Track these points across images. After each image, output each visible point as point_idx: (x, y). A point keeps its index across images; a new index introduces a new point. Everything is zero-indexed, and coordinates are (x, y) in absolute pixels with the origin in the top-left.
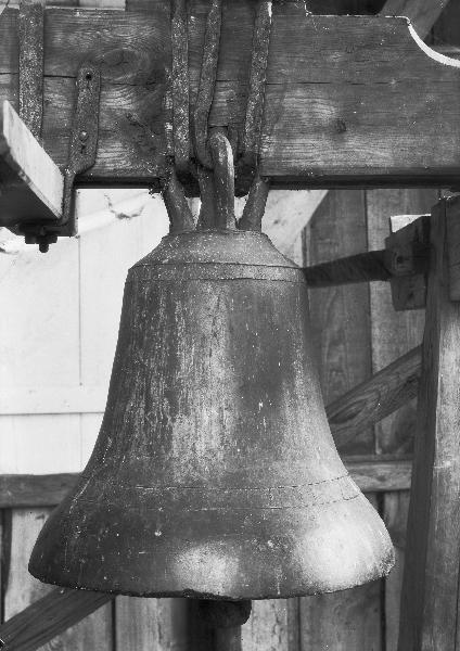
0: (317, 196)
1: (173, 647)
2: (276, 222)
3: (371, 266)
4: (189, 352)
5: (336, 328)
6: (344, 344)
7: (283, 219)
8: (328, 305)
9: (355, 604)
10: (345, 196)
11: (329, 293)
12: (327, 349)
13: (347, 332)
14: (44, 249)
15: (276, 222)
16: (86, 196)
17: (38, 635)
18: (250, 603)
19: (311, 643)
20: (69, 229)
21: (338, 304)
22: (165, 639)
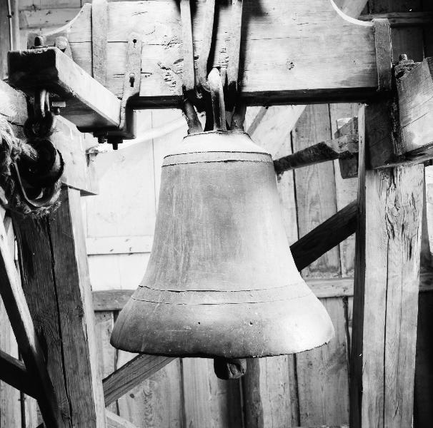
0: (299, 109)
1: (219, 394)
2: (272, 129)
3: (322, 153)
4: (198, 207)
5: (314, 194)
6: (320, 204)
7: (276, 127)
8: (308, 179)
9: (331, 367)
10: (320, 108)
11: (309, 170)
12: (309, 208)
13: (321, 196)
14: (115, 148)
15: (272, 129)
16: (141, 116)
17: (128, 383)
18: (95, 292)
19: (305, 392)
20: (131, 137)
21: (315, 179)
22: (213, 390)
